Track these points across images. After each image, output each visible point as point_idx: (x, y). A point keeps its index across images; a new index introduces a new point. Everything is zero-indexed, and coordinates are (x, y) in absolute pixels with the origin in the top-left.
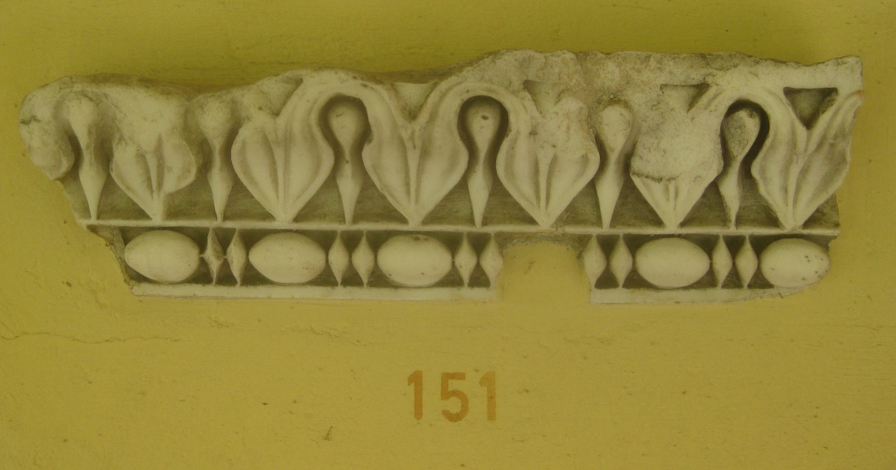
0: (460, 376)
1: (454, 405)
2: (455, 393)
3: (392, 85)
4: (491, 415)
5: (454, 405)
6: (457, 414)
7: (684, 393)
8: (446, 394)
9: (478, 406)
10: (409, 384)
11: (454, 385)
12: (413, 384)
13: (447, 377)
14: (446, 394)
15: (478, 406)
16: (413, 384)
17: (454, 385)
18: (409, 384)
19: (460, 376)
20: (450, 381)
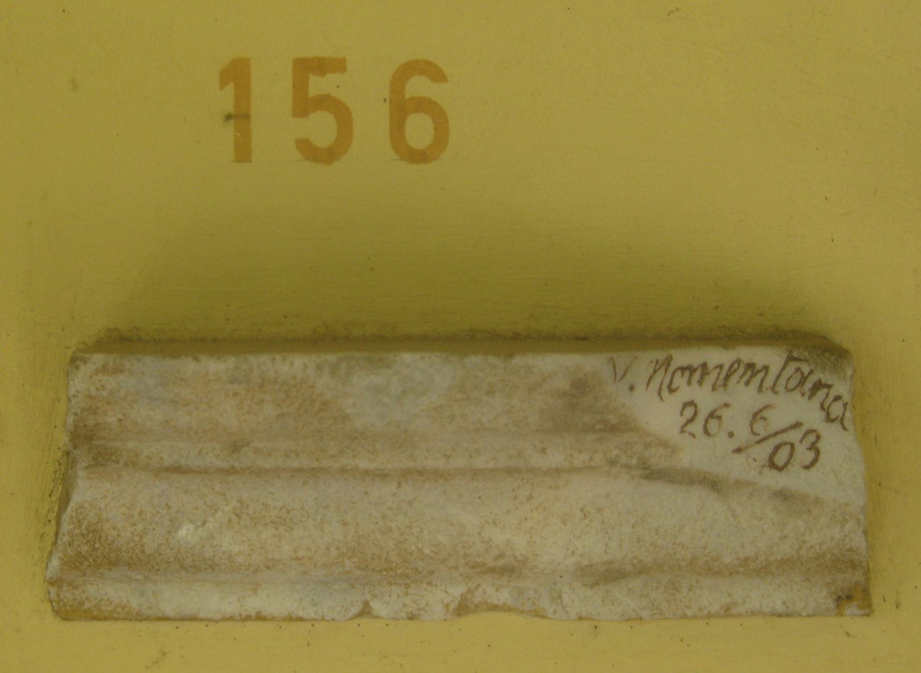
1: (321, 128)
2: (326, 102)
5: (321, 128)
8: (304, 105)
9: (272, 91)
10: (222, 86)
11: (318, 85)
12: (230, 87)
13: (307, 67)
14: (304, 105)
15: (272, 91)
16: (230, 87)
17: (318, 85)
18: (222, 86)
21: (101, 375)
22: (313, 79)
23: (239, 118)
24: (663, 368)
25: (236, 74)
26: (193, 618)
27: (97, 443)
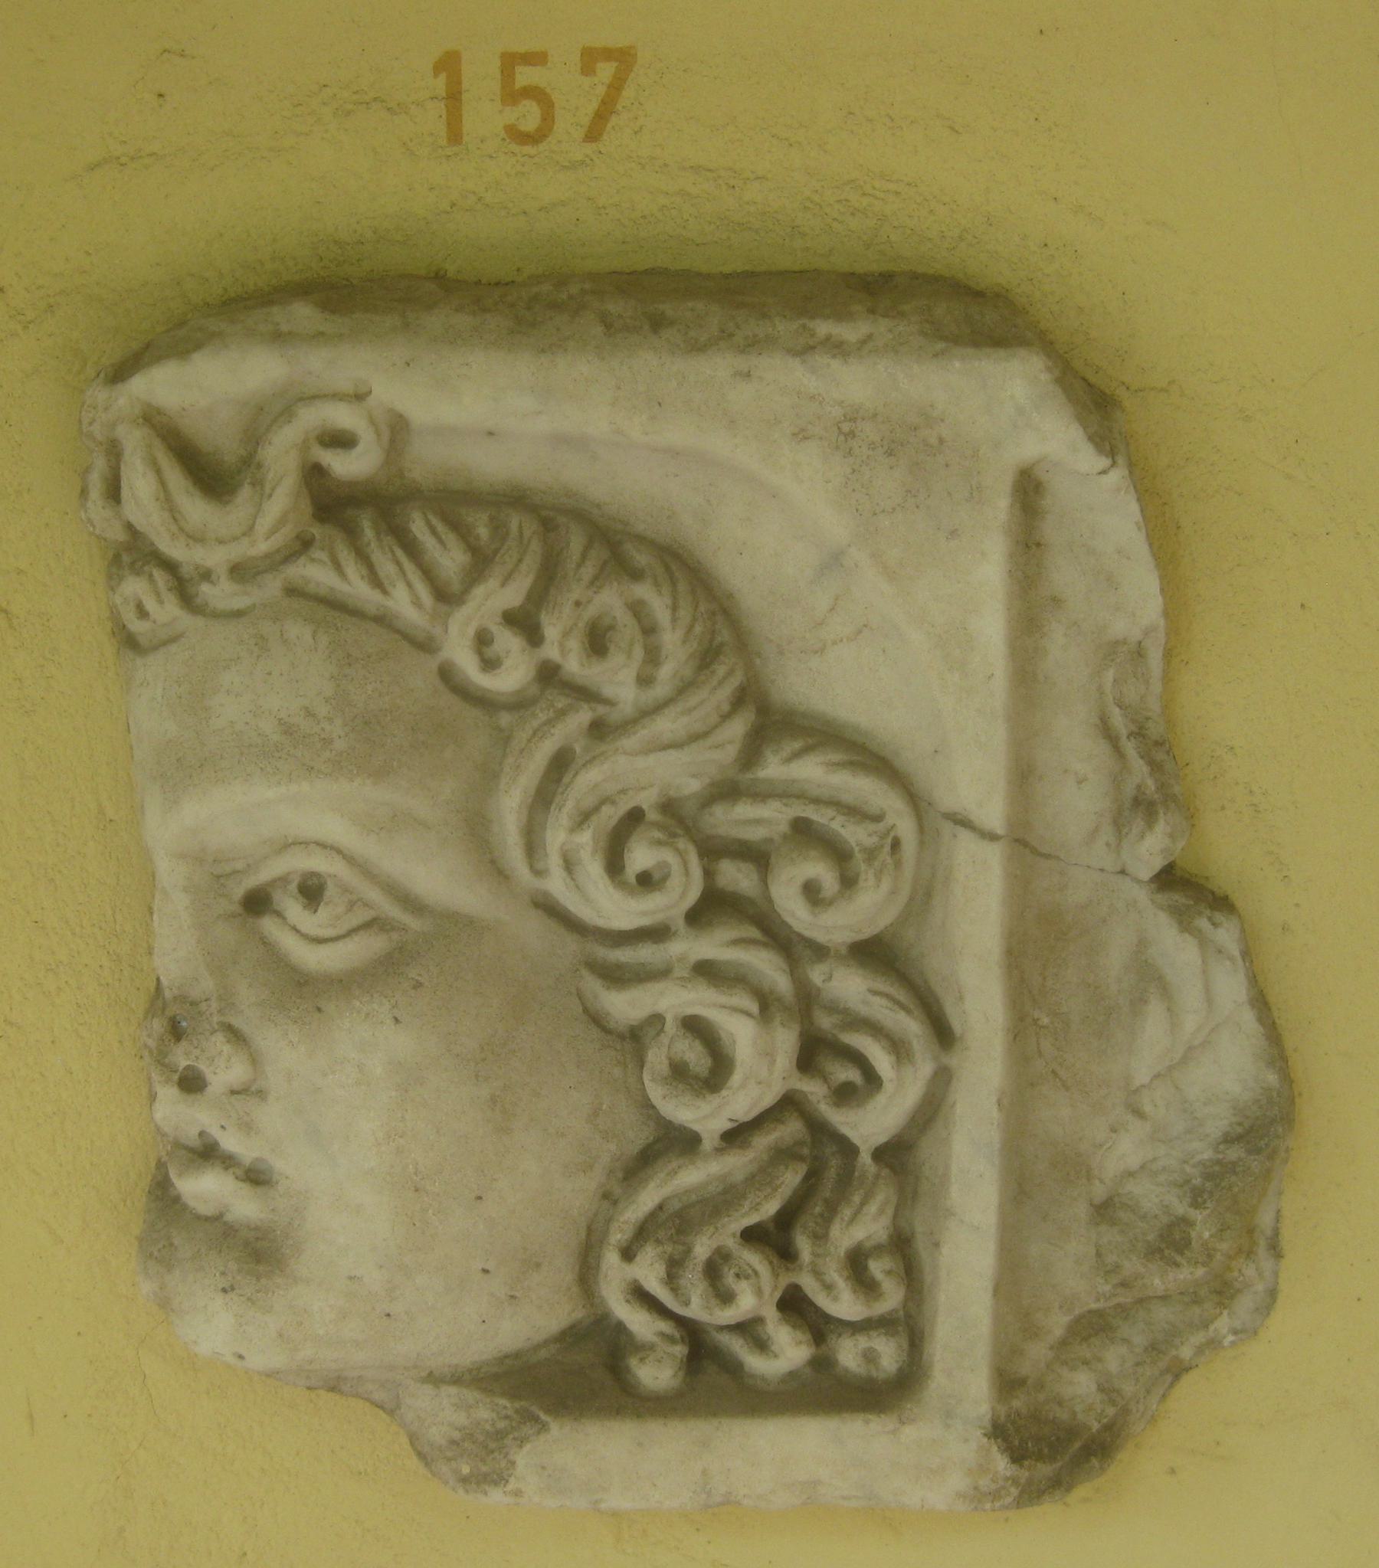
0: (536, 59)
1: (529, 116)
2: (533, 93)
3: (605, 563)
4: (449, 64)
5: (529, 116)
6: (539, 129)
7: (161, 95)
8: (512, 95)
9: (481, 76)
10: (436, 75)
11: (526, 76)
12: (443, 76)
13: (510, 62)
14: (512, 95)
15: (481, 76)
16: (443, 76)
17: (526, 76)
18: (436, 75)
19: (536, 59)
20: (519, 69)
21: (835, 1231)
22: (519, 69)
23: (454, 97)
24: (663, 1216)
25: (449, 64)
26: (314, 397)
27: (1009, 1500)
